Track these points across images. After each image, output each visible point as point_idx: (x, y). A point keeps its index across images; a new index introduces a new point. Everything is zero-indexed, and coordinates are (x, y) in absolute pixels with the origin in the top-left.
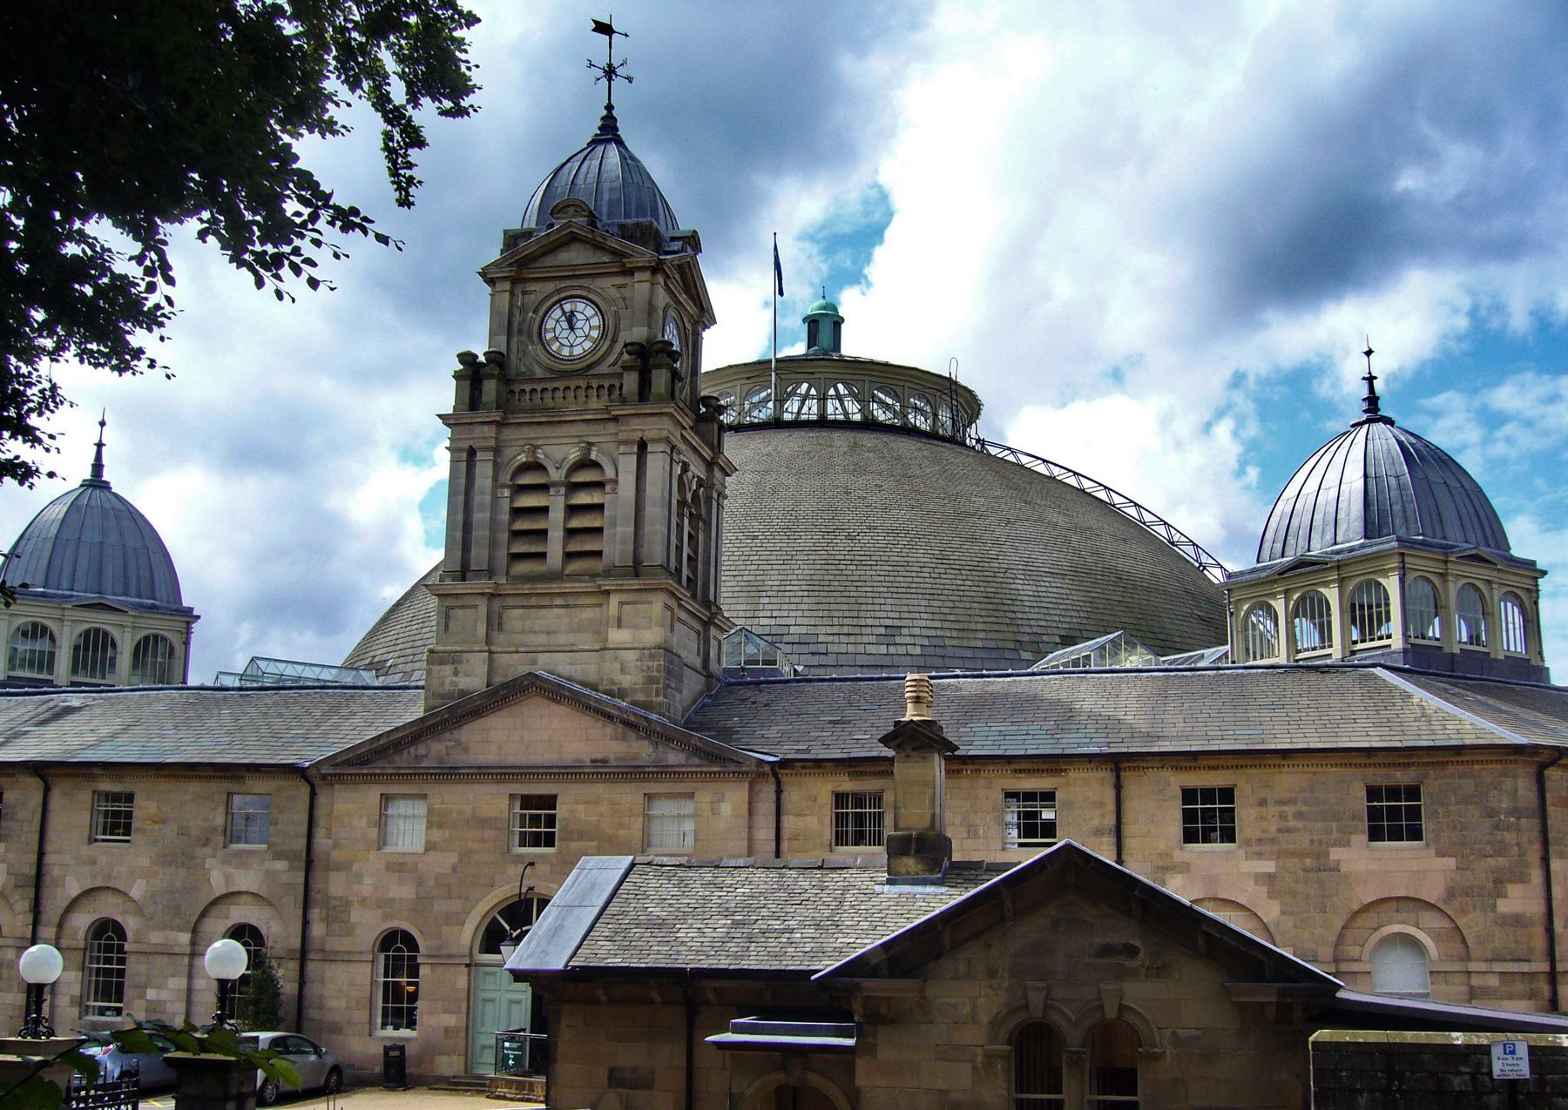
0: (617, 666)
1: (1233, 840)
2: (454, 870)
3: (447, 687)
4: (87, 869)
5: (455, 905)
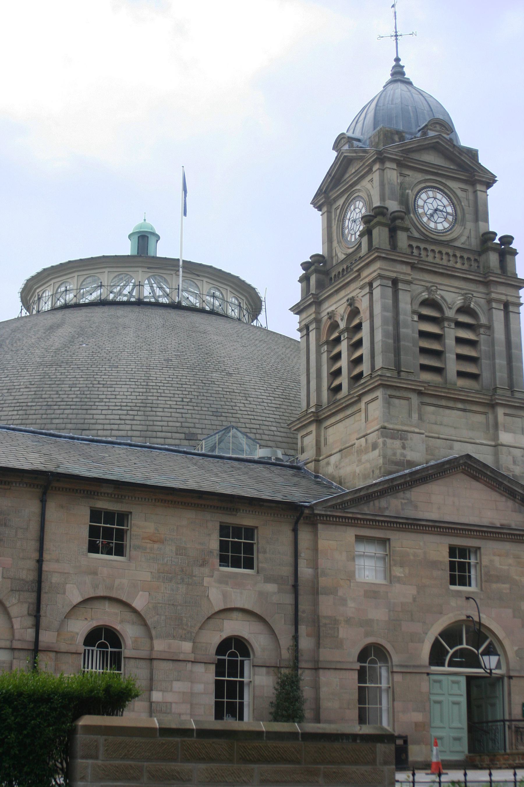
0: (510, 459)
1: (252, 568)
2: (414, 599)
3: (398, 457)
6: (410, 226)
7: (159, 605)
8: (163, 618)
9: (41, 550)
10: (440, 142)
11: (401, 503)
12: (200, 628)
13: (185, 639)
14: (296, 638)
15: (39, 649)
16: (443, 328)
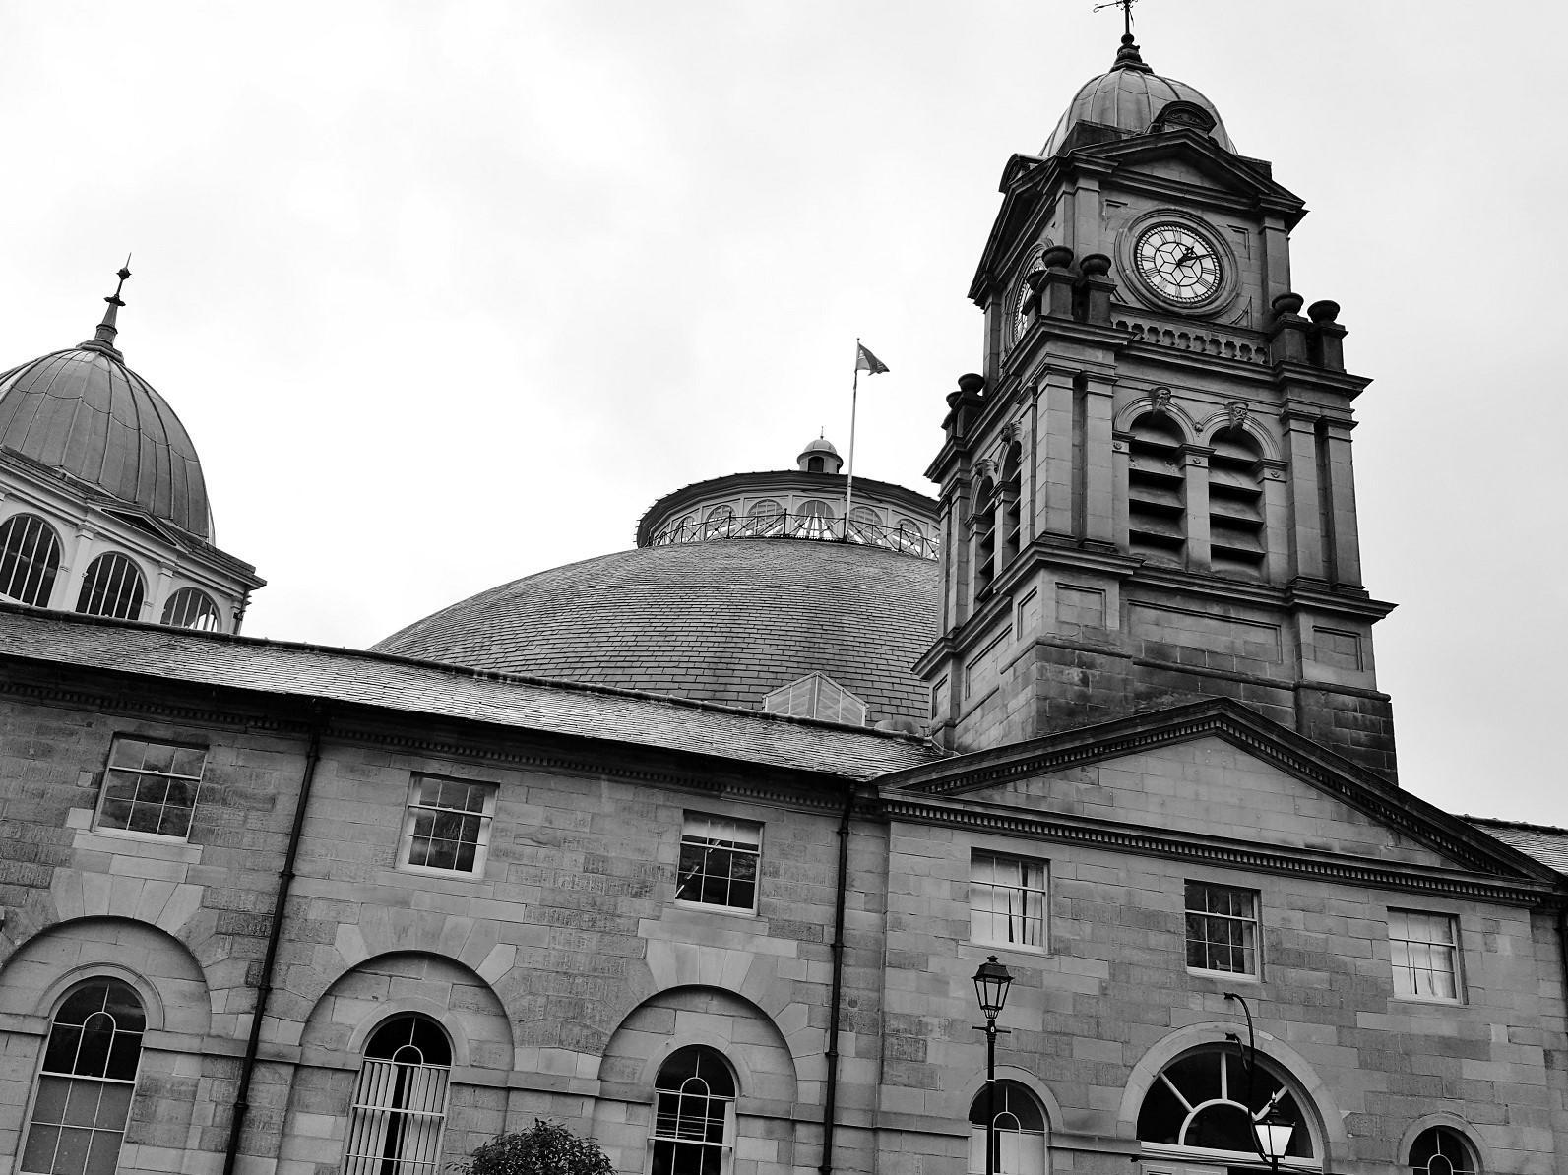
4: (387, 915)
5: (1110, 1052)
6: (1118, 282)
7: (535, 974)
8: (541, 1000)
9: (292, 854)
10: (1189, 142)
11: (1078, 790)
12: (621, 1027)
13: (585, 1050)
14: (832, 1057)
15: (259, 1057)
16: (1182, 469)
